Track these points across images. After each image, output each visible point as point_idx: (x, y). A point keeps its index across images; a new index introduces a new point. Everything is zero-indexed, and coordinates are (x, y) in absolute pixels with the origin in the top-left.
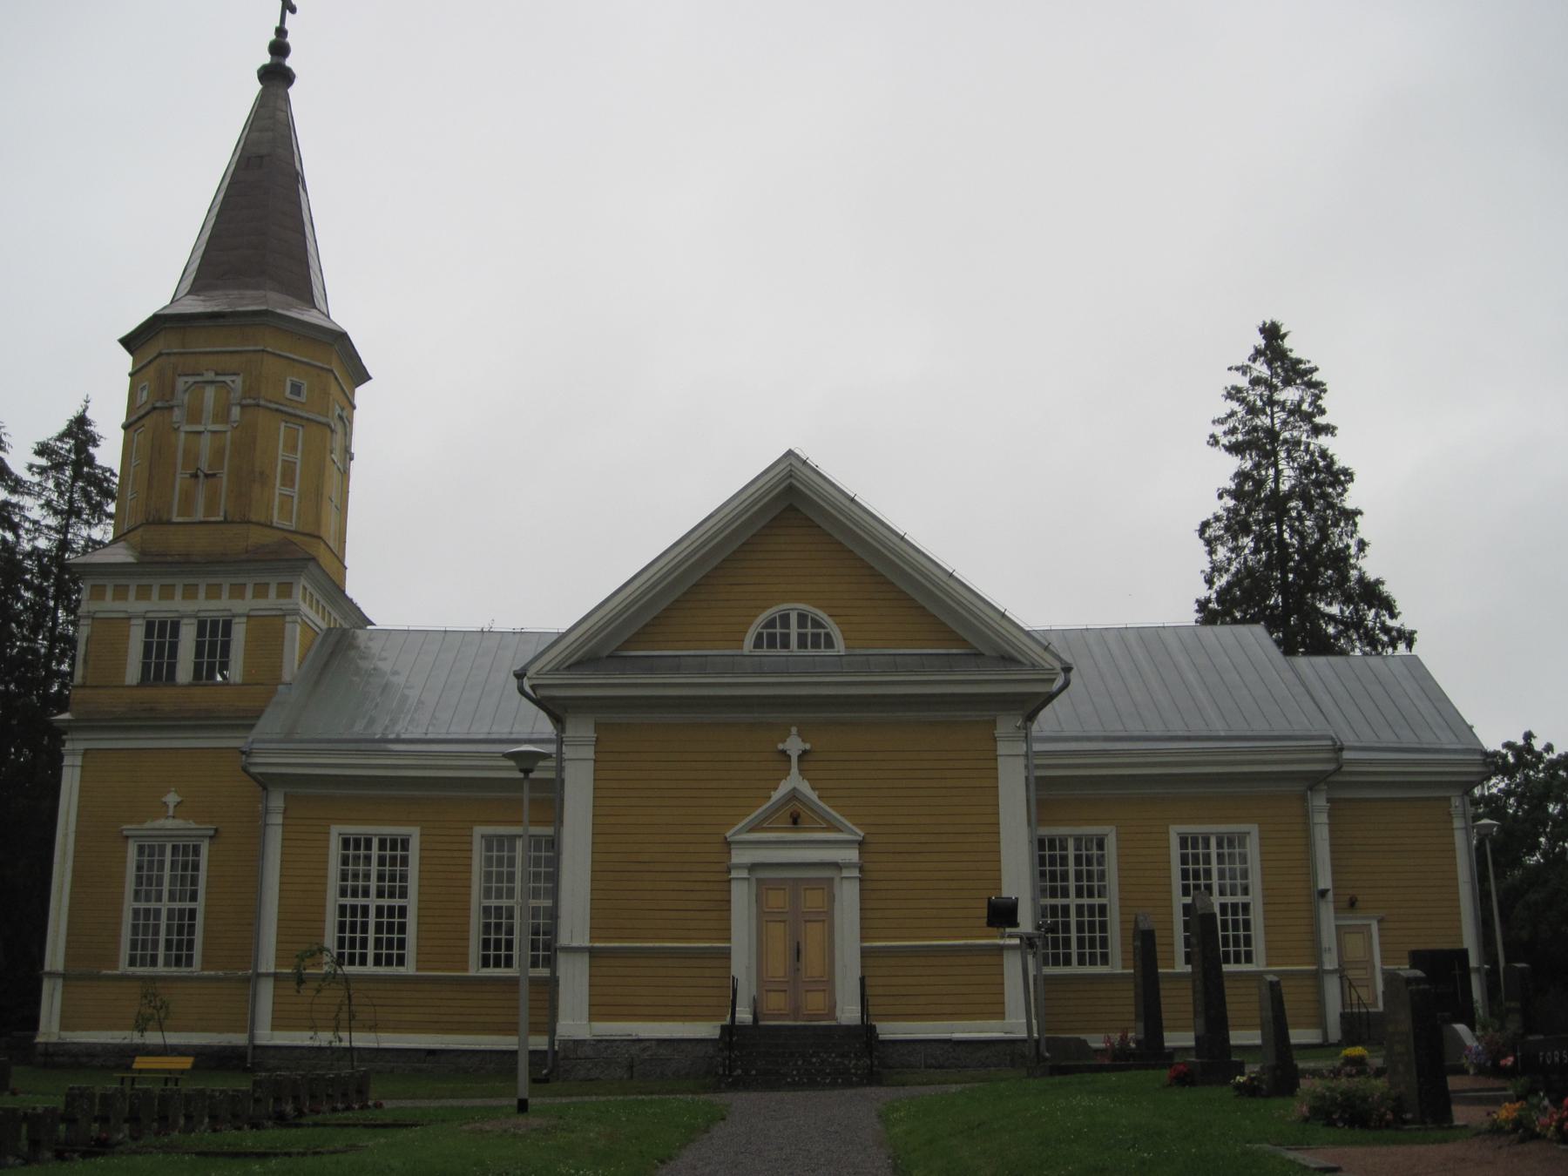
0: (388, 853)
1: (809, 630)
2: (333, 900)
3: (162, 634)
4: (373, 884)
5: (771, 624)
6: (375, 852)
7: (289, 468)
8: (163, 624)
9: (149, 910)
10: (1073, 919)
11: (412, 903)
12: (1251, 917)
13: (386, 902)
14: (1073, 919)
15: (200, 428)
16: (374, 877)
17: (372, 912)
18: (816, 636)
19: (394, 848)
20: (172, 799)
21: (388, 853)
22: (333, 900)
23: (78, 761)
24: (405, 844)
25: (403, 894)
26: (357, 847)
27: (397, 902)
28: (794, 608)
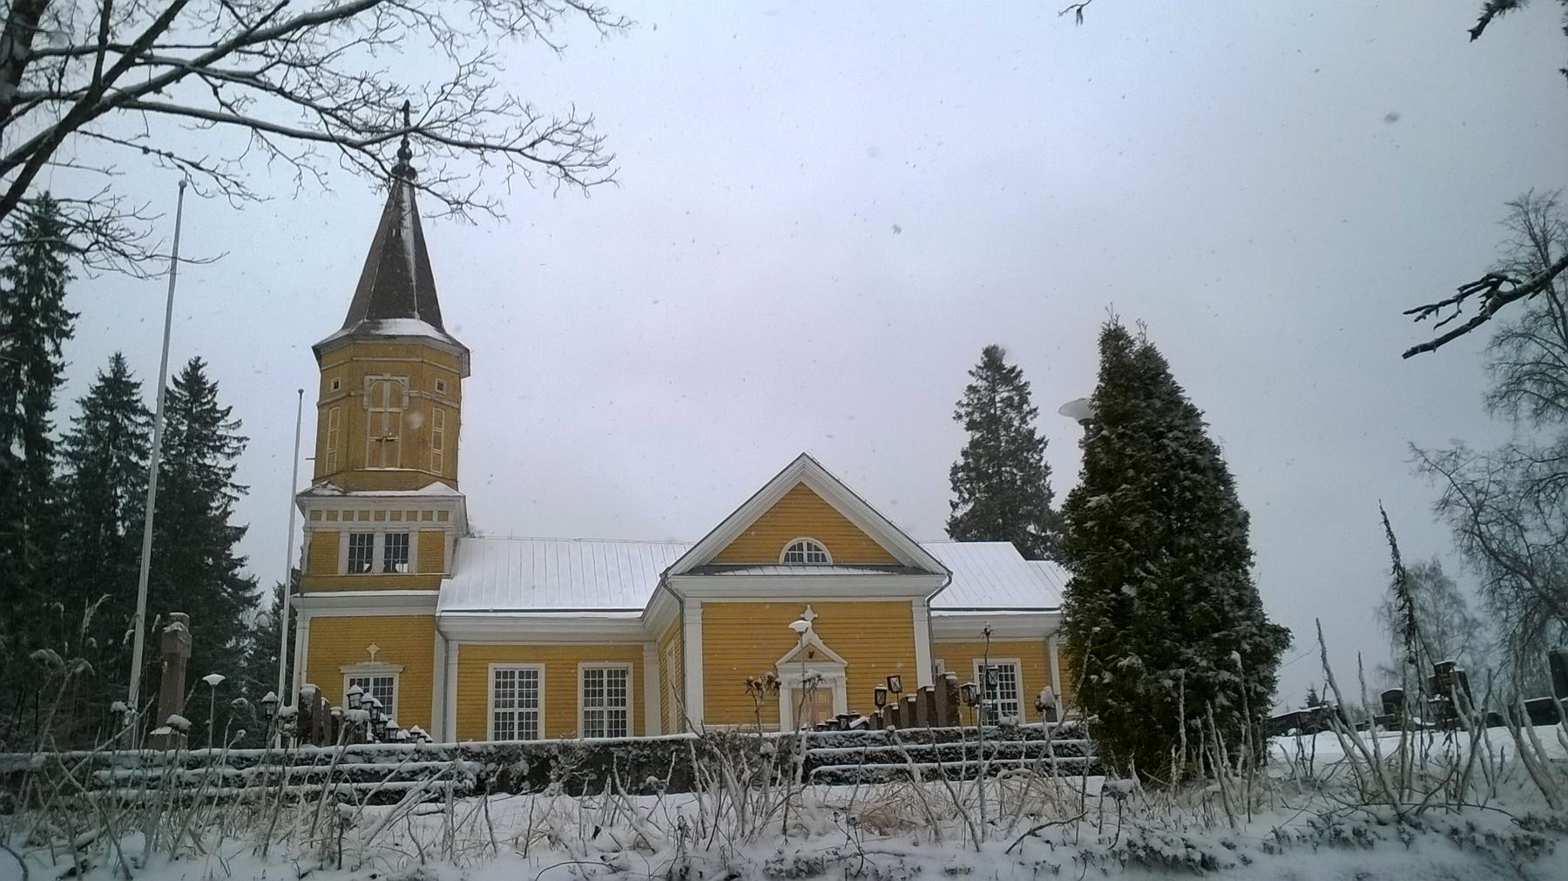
0: (502, 680)
1: (813, 552)
2: (491, 710)
3: (397, 543)
4: (516, 699)
5: (793, 548)
6: (517, 679)
7: (438, 437)
8: (362, 536)
9: (506, 713)
10: (516, 721)
11: (541, 710)
12: (1017, 690)
13: (524, 710)
14: (516, 721)
15: (382, 410)
16: (516, 695)
17: (516, 716)
18: (817, 555)
19: (616, 676)
20: (373, 649)
21: (502, 680)
22: (491, 710)
23: (307, 625)
24: (535, 674)
25: (535, 705)
26: (616, 676)
27: (532, 710)
28: (805, 540)
